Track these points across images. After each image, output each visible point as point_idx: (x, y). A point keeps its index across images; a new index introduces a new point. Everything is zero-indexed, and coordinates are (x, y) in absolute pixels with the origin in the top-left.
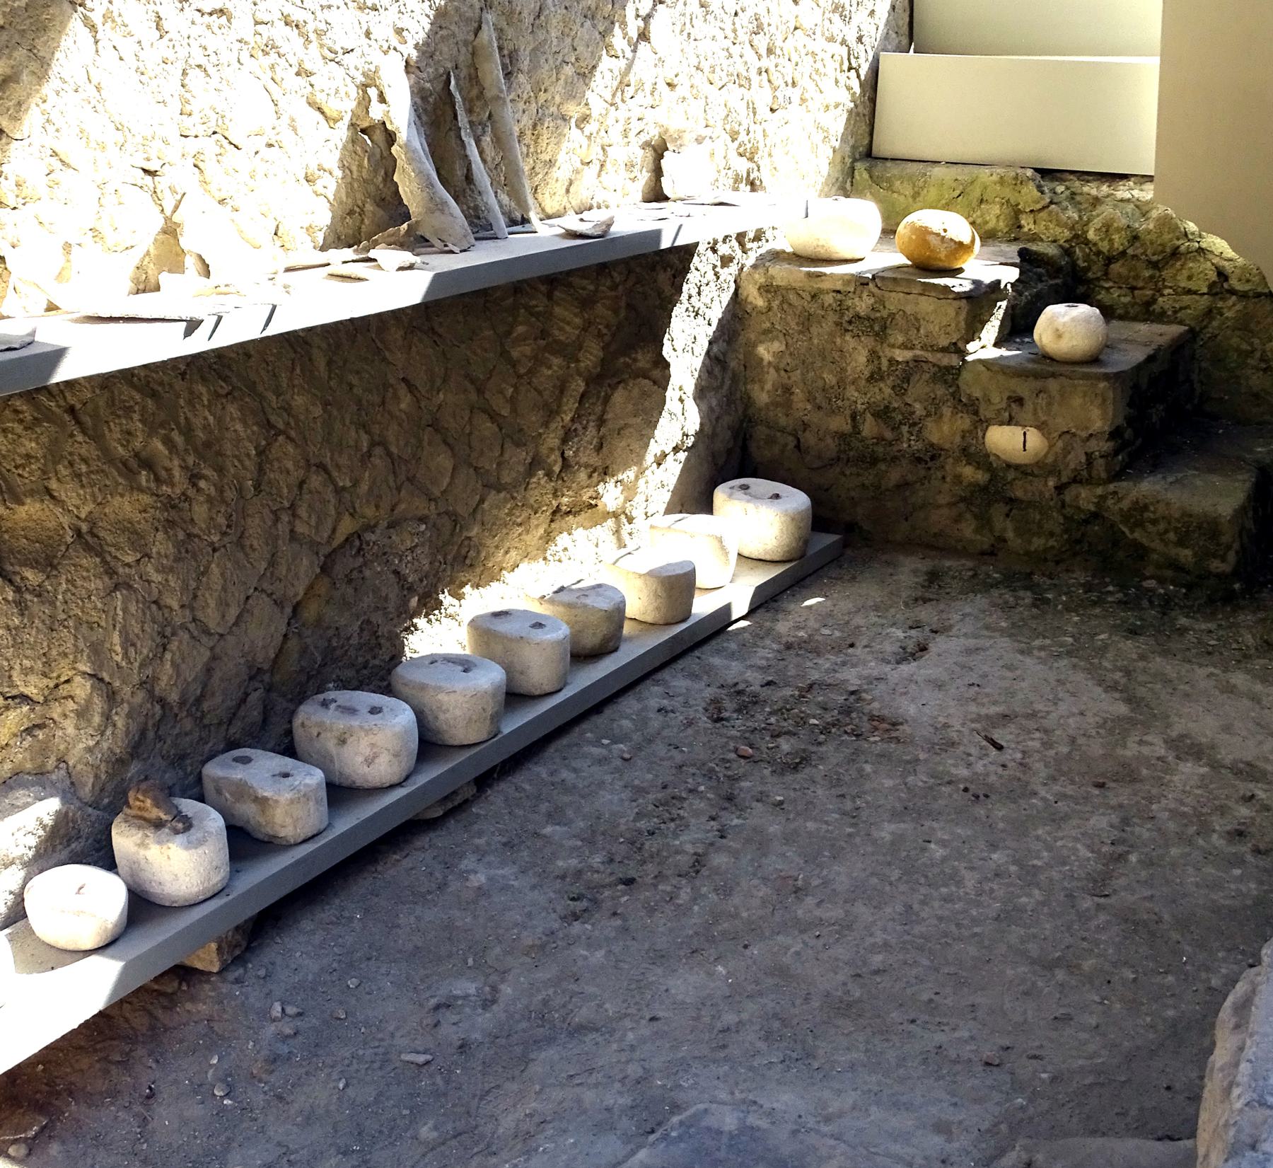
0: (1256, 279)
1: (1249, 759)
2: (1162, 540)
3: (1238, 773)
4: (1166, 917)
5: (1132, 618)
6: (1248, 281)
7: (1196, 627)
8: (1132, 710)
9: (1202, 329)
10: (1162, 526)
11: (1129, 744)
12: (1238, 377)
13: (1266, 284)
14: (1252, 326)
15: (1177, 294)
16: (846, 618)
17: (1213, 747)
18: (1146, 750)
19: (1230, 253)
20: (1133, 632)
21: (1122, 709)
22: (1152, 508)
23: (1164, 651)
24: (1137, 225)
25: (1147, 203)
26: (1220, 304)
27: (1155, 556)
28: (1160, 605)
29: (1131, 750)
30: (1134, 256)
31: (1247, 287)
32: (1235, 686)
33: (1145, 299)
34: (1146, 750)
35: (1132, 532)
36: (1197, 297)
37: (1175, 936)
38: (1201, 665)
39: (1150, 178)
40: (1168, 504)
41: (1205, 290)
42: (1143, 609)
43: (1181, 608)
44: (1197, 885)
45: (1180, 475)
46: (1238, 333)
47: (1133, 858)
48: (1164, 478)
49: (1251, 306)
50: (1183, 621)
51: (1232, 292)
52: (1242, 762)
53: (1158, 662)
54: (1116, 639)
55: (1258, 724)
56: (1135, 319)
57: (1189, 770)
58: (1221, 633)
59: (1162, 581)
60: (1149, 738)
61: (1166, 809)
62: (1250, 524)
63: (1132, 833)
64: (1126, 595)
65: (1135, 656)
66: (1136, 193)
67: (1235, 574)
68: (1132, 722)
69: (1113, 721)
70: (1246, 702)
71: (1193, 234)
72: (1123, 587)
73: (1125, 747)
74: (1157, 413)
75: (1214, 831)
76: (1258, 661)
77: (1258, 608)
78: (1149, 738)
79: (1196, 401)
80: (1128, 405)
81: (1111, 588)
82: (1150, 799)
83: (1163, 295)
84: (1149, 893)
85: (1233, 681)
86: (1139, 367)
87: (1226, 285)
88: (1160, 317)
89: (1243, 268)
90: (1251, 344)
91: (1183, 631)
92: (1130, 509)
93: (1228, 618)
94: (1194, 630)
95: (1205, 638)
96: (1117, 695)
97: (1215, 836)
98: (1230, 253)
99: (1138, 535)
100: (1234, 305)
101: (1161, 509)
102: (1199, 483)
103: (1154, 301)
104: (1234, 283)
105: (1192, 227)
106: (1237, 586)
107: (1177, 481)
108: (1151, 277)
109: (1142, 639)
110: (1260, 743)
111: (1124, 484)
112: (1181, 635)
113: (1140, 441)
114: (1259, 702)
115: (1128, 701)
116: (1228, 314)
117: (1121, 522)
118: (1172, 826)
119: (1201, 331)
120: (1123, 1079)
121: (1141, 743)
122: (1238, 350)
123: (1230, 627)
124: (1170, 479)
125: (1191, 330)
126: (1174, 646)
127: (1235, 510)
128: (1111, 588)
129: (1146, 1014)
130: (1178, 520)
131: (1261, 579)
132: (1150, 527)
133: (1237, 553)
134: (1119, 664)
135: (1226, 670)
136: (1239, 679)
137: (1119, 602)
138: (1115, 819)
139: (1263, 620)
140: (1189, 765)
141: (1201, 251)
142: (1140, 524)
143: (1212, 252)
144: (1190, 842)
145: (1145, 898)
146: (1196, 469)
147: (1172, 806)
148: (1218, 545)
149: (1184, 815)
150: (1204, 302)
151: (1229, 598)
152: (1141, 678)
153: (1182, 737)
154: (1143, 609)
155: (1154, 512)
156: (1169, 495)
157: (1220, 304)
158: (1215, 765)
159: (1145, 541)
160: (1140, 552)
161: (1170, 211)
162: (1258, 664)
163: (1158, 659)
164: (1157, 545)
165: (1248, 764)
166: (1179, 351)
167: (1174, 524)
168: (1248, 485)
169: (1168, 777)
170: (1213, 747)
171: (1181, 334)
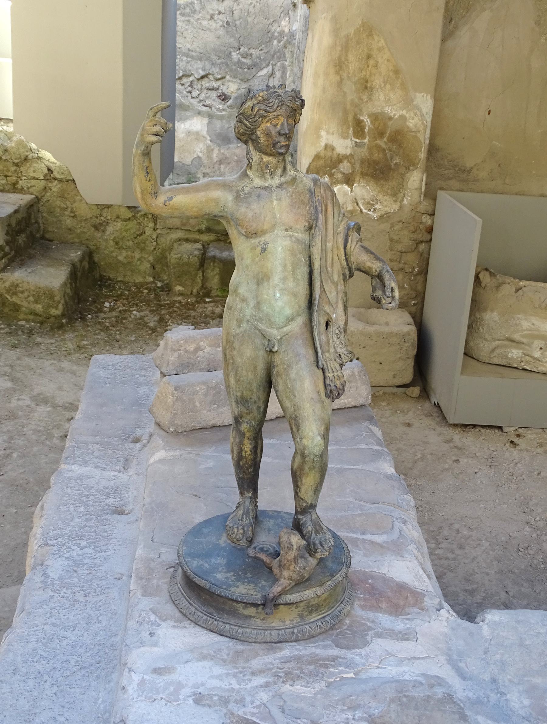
0: (66, 172)
1: (71, 401)
2: (27, 301)
3: (65, 408)
4: (31, 480)
5: (13, 340)
6: (62, 173)
7: (45, 342)
8: (14, 385)
9: (42, 197)
10: (26, 294)
11: (13, 401)
12: (61, 221)
13: (71, 176)
14: (66, 195)
15: (28, 179)
16: (453, 521)
17: (53, 398)
18: (21, 403)
19: (53, 159)
20: (14, 347)
21: (9, 384)
22: (20, 285)
23: (29, 354)
24: (6, 144)
25: (11, 133)
26: (50, 185)
27: (24, 309)
28: (28, 333)
29: (14, 403)
30: (6, 160)
31: (62, 177)
32: (63, 368)
33: (13, 182)
34: (21, 403)
35: (12, 298)
36: (39, 181)
37: (36, 488)
38: (47, 360)
39: (10, 121)
40: (28, 283)
41: (42, 178)
42: (19, 335)
43: (38, 333)
44: (46, 463)
45: (34, 269)
46: (59, 199)
47: (15, 455)
48: (26, 270)
49: (64, 186)
50: (39, 340)
51: (55, 179)
52: (67, 403)
53: (27, 360)
54: (6, 350)
55: (75, 385)
56: (8, 192)
57: (42, 409)
58: (57, 344)
59: (28, 321)
60: (23, 397)
61: (31, 430)
62: (69, 291)
63: (14, 443)
64: (10, 329)
65: (15, 358)
66: (5, 128)
67: (63, 315)
68: (14, 390)
69: (4, 391)
70: (70, 375)
71: (34, 149)
72: (9, 325)
73: (10, 402)
74: (22, 239)
75: (54, 437)
76: (74, 355)
77: (74, 331)
78: (23, 397)
79: (41, 233)
80: (6, 234)
81: (2, 326)
82: (23, 426)
83: (21, 180)
84: (23, 470)
85: (62, 366)
86: (10, 216)
87: (52, 175)
88: (21, 191)
89: (60, 167)
90: (66, 204)
91: (39, 344)
92: (10, 286)
93: (60, 337)
94: (44, 343)
95: (50, 347)
96: (6, 378)
97: (54, 439)
98: (53, 159)
99: (14, 299)
100: (56, 185)
101: (25, 286)
102: (43, 272)
103: (17, 183)
104: (56, 174)
105: (33, 146)
106: (64, 321)
107: (32, 272)
108: (16, 171)
109: (18, 350)
110: (75, 393)
111: (6, 274)
112: (38, 346)
113: (13, 253)
114: (75, 375)
115: (12, 380)
116: (54, 189)
117: (6, 293)
118: (34, 437)
119: (41, 198)
120: (10, 560)
121: (18, 399)
122: (59, 207)
123: (61, 341)
124: (29, 271)
125: (37, 197)
126: (34, 351)
127: (61, 284)
128: (2, 326)
129: (22, 527)
130: (34, 291)
131: (76, 317)
132: (20, 295)
133: (63, 305)
134: (7, 363)
135: (60, 361)
136: (65, 364)
137: (7, 333)
138: (5, 438)
139: (77, 336)
140: (42, 407)
141: (39, 158)
142: (15, 294)
143: (44, 159)
144: (43, 444)
145: (21, 473)
146: (42, 265)
147: (34, 427)
148: (54, 301)
149: (40, 431)
150: (42, 184)
151: (61, 327)
152: (18, 369)
153: (39, 394)
154: (19, 335)
155: (22, 287)
156: (29, 279)
157: (50, 185)
158: (54, 406)
159: (18, 302)
160: (16, 308)
161: (22, 138)
162: (75, 356)
163: (26, 359)
164: (24, 303)
165: (71, 404)
166: (31, 206)
167: (32, 292)
168: (67, 272)
169: (32, 414)
170: (53, 398)
171: (32, 200)
